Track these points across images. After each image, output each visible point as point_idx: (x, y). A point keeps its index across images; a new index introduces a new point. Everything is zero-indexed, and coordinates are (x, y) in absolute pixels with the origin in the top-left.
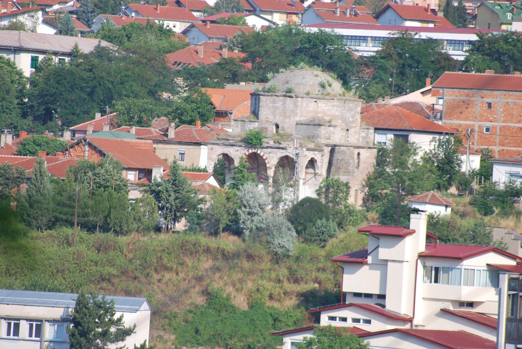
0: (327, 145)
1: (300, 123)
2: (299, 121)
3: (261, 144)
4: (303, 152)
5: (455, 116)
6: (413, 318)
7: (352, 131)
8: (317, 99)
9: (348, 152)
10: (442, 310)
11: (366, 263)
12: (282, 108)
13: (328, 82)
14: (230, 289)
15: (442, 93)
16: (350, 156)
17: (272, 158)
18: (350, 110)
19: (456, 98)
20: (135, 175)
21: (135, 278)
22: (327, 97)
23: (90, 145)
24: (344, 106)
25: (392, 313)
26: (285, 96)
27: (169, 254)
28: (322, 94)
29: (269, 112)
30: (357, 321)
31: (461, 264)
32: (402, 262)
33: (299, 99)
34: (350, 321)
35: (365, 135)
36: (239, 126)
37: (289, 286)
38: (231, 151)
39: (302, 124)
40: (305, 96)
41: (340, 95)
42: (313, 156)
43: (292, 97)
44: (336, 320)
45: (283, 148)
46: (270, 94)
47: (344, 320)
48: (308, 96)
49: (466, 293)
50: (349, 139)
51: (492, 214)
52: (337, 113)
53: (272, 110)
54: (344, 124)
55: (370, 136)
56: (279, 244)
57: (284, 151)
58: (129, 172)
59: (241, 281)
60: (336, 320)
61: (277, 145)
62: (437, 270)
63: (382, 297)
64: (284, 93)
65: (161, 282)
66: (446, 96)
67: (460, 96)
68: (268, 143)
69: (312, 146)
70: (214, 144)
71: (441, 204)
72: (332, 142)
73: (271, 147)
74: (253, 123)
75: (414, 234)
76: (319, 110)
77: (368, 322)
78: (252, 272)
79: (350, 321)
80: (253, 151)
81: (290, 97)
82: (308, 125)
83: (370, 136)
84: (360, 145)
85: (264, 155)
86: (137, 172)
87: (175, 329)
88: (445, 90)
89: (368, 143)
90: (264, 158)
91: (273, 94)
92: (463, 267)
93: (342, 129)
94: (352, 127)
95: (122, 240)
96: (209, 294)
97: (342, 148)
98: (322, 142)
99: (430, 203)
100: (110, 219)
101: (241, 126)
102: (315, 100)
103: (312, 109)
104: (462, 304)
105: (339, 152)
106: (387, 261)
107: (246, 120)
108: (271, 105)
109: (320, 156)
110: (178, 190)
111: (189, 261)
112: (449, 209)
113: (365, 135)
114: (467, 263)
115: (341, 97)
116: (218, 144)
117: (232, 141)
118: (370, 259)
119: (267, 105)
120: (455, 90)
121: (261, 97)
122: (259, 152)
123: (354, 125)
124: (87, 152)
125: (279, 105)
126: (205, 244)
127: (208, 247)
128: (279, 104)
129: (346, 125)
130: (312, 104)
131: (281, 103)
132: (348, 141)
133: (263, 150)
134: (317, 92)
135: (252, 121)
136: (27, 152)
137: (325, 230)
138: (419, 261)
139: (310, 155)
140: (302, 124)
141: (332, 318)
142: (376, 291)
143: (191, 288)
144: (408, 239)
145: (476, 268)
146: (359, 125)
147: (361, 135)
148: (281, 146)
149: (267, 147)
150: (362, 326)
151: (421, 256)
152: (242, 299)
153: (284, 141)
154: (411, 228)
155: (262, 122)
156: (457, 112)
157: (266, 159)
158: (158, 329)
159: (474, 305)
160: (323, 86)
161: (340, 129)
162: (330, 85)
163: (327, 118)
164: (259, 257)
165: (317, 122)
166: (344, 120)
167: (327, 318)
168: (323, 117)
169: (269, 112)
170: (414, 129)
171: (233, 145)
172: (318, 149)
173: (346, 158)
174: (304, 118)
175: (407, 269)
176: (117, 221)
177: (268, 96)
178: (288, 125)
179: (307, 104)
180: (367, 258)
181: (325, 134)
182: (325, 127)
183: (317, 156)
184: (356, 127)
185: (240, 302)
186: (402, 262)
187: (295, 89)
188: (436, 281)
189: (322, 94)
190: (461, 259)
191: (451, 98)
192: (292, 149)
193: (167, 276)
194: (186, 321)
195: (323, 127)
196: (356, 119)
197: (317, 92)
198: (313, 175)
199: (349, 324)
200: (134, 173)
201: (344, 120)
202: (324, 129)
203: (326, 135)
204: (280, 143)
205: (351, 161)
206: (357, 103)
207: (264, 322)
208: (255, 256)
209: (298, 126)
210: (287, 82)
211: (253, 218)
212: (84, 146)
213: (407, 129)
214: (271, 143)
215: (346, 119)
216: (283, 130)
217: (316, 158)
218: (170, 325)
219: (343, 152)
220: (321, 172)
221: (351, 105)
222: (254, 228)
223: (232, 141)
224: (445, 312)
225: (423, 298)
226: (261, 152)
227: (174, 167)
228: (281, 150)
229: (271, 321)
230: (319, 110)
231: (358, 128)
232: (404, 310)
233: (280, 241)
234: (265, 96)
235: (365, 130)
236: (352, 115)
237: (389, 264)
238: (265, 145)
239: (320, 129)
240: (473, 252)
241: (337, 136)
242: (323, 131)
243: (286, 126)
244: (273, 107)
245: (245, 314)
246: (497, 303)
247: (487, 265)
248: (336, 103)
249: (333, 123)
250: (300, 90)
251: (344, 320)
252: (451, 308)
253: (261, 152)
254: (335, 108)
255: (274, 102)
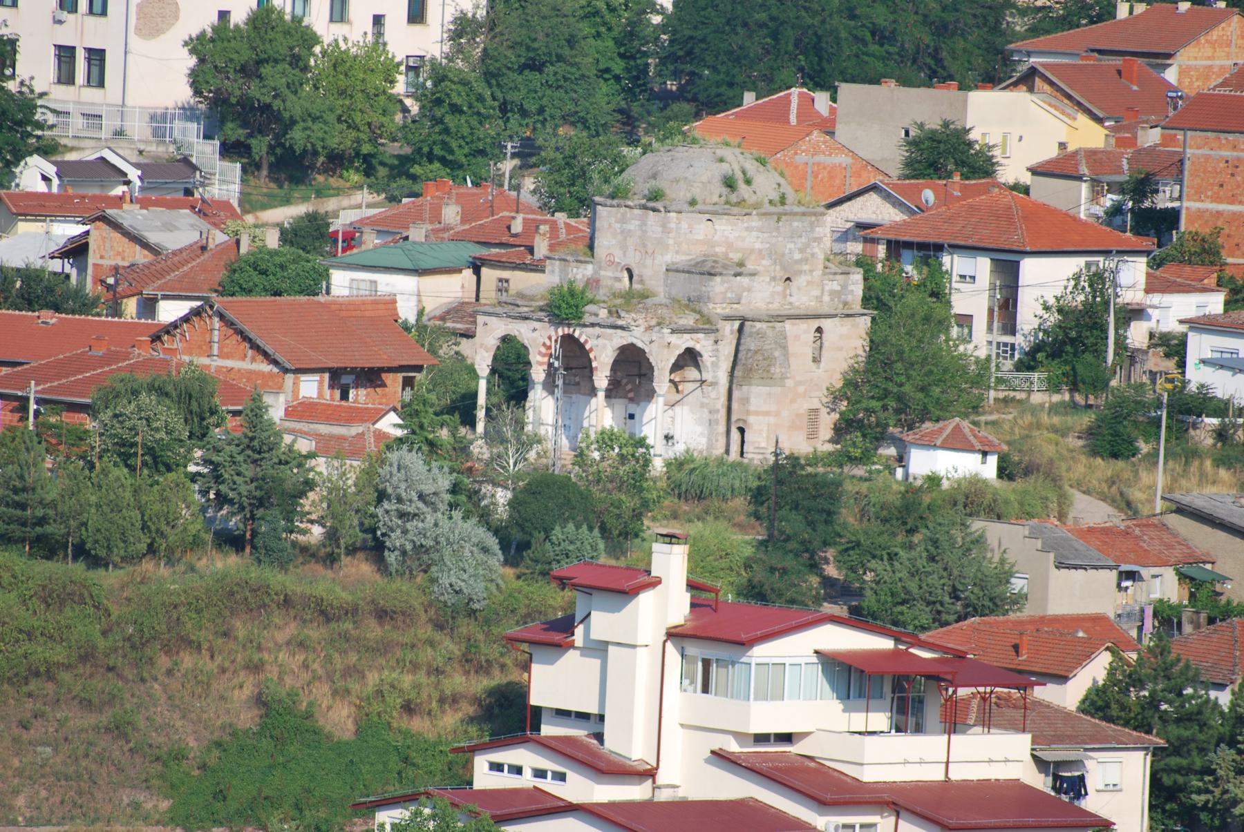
0: (728, 318)
1: (674, 267)
2: (673, 263)
3: (580, 318)
4: (663, 337)
5: (1209, 193)
6: (657, 768)
7: (800, 281)
8: (713, 214)
9: (770, 333)
10: (713, 752)
11: (571, 646)
12: (639, 233)
13: (744, 173)
14: (322, 692)
15: (1181, 143)
16: (776, 343)
17: (603, 351)
18: (794, 235)
19: (1212, 152)
20: (321, 382)
21: (110, 669)
22: (735, 210)
23: (222, 317)
24: (777, 229)
25: (613, 757)
26: (644, 207)
27: (198, 611)
28: (727, 203)
29: (614, 242)
30: (540, 774)
31: (749, 654)
32: (634, 646)
33: (673, 215)
34: (528, 773)
35: (839, 288)
36: (557, 270)
37: (457, 681)
38: (522, 330)
39: (677, 271)
40: (686, 207)
41: (771, 202)
42: (690, 344)
43: (659, 211)
44: (502, 771)
45: (622, 328)
46: (615, 202)
47: (518, 770)
48: (691, 209)
49: (767, 717)
50: (792, 299)
51: (1134, 455)
52: (758, 246)
53: (620, 237)
54: (778, 268)
55: (851, 287)
56: (451, 585)
57: (625, 334)
58: (304, 377)
59: (348, 672)
60: (502, 771)
61: (612, 320)
62: (707, 664)
63: (601, 718)
64: (644, 201)
65: (173, 675)
66: (1191, 147)
67: (1220, 148)
68: (596, 315)
69: (689, 320)
70: (490, 314)
71: (970, 449)
72: (741, 309)
73: (599, 325)
74: (583, 266)
75: (659, 587)
76: (716, 238)
77: (561, 777)
78: (383, 648)
79: (528, 773)
80: (566, 331)
81: (654, 210)
82: (689, 272)
83: (851, 287)
84: (826, 310)
85: (586, 341)
86: (327, 376)
87: (173, 786)
88: (1189, 133)
89: (845, 304)
90: (587, 347)
91: (622, 202)
92: (753, 662)
93: (774, 279)
94: (801, 272)
95: (109, 578)
96: (265, 704)
97: (758, 325)
98: (719, 311)
99: (946, 446)
100: (87, 530)
101: (561, 271)
102: (708, 216)
103: (701, 237)
104: (761, 738)
105: (751, 335)
106: (607, 643)
107: (568, 258)
108: (618, 225)
109: (711, 342)
110: (261, 459)
111: (241, 628)
112: (993, 460)
113: (839, 288)
114: (762, 652)
115: (773, 209)
116: (497, 315)
117: (526, 309)
118: (579, 635)
119: (610, 225)
120: (1209, 134)
121: (599, 208)
122: (576, 335)
123: (806, 267)
124: (216, 333)
125: (632, 228)
126: (279, 588)
127: (286, 595)
128: (633, 225)
129: (784, 268)
130: (702, 226)
131: (637, 223)
132: (791, 303)
133: (585, 329)
134: (715, 199)
135: (581, 262)
136: (237, 288)
137: (571, 548)
138: (669, 644)
139: (682, 343)
140: (677, 271)
141: (497, 767)
142: (593, 709)
143: (234, 688)
144: (646, 599)
145: (787, 661)
146: (821, 266)
147: (827, 288)
148: (620, 323)
149: (593, 325)
150: (548, 785)
151: (673, 635)
152: (345, 713)
153: (627, 312)
154: (653, 574)
155: (600, 262)
156: (1213, 184)
157: (591, 350)
158: (134, 787)
159: (794, 738)
160: (730, 183)
161: (768, 279)
162: (748, 182)
163: (736, 257)
164: (403, 614)
165: (707, 267)
166: (778, 257)
167: (487, 766)
168: (726, 254)
169: (614, 242)
170: (1028, 249)
171: (527, 318)
172: (707, 326)
173: (766, 347)
174: (684, 258)
175: (645, 662)
176: (99, 536)
177: (612, 206)
178: (652, 273)
179: (690, 227)
180: (573, 634)
181: (725, 293)
182: (725, 278)
183: (702, 344)
184: (811, 271)
185: (339, 719)
186: (634, 646)
187: (668, 192)
188: (706, 689)
189: (727, 203)
190: (746, 644)
191: (1200, 152)
192: (642, 329)
193: (187, 660)
194: (203, 767)
195: (718, 279)
196: (813, 255)
197: (715, 199)
198: (698, 384)
199: (527, 781)
200: (316, 377)
201: (778, 257)
202: (723, 282)
203: (729, 295)
204: (619, 317)
205: (777, 354)
206: (813, 218)
207: (380, 767)
208: (395, 612)
209: (670, 274)
210: (654, 176)
211: (409, 526)
212: (210, 317)
213: (1015, 248)
214: (603, 313)
215: (783, 255)
216: (641, 282)
217: (698, 347)
218: (161, 776)
219: (761, 335)
220: (715, 377)
221: (796, 224)
222: (409, 547)
223: (526, 309)
224: (720, 757)
225: (682, 725)
226: (581, 335)
227: (252, 410)
228: (619, 331)
229: (394, 763)
230: (716, 238)
231: (818, 273)
232: (638, 751)
233: (453, 580)
234: (605, 206)
235: (838, 277)
236: (799, 245)
237: (610, 647)
238: (588, 319)
239: (712, 283)
240: (776, 628)
241: (760, 295)
242: (718, 286)
243: (647, 273)
244: (622, 232)
245: (340, 748)
246: (863, 730)
247: (816, 652)
248: (755, 222)
249: (750, 266)
250: (678, 194)
251: (518, 770)
252: (733, 747)
253: (581, 335)
254: (755, 234)
255: (623, 221)
